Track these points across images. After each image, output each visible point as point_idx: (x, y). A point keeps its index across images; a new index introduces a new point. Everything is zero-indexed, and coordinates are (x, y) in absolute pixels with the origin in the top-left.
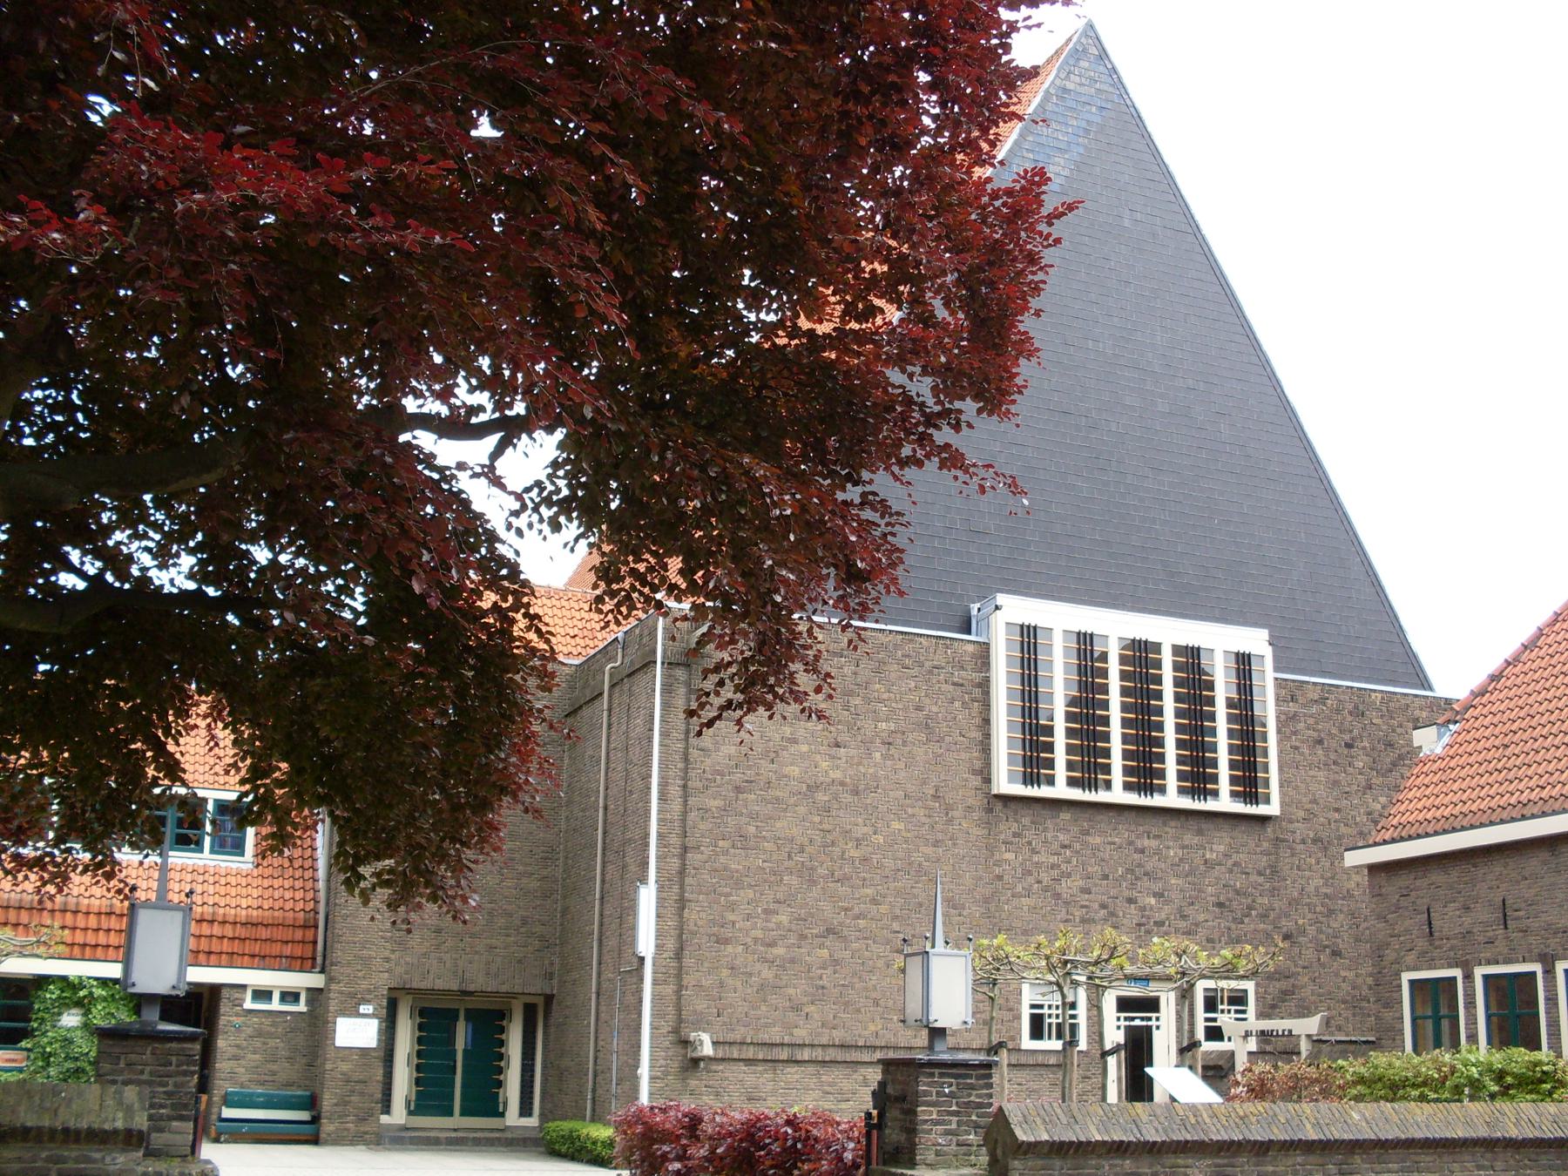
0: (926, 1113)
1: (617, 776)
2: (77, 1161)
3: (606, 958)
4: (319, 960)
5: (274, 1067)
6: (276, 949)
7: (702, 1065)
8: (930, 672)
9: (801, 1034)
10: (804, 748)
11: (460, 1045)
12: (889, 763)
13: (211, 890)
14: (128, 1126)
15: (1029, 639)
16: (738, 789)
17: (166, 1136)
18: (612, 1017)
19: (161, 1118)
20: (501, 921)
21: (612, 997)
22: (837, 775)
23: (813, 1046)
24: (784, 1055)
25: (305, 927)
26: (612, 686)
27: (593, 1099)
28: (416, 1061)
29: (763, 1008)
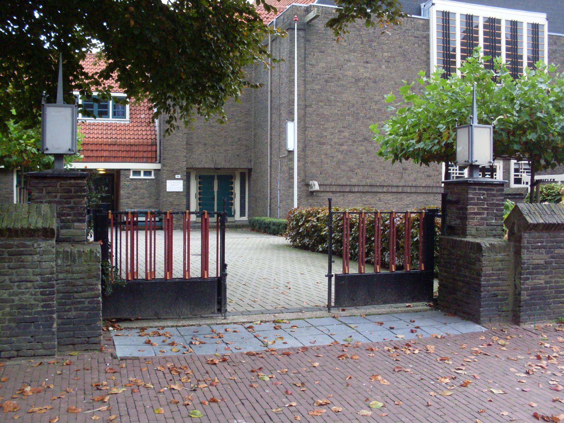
0: (472, 209)
1: (276, 79)
2: (18, 246)
3: (274, 152)
4: (158, 158)
5: (143, 201)
6: (141, 155)
7: (315, 194)
8: (405, 32)
9: (354, 181)
10: (353, 64)
11: (216, 189)
12: (388, 70)
13: (114, 132)
14: (44, 226)
15: (446, 17)
16: (327, 81)
17: (72, 231)
18: (277, 176)
19: (68, 221)
20: (230, 140)
21: (277, 168)
22: (367, 75)
23: (359, 186)
24: (347, 189)
25: (152, 145)
26: (272, 41)
27: (270, 209)
28: (198, 196)
29: (339, 171)
